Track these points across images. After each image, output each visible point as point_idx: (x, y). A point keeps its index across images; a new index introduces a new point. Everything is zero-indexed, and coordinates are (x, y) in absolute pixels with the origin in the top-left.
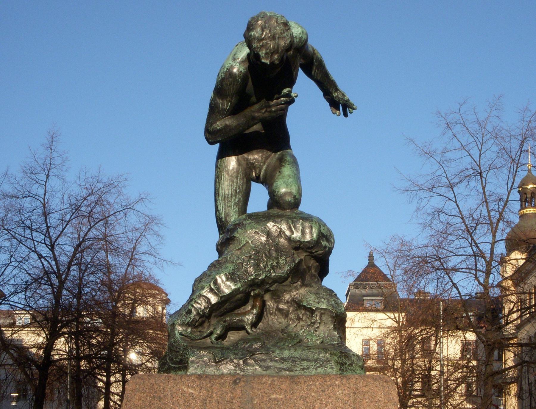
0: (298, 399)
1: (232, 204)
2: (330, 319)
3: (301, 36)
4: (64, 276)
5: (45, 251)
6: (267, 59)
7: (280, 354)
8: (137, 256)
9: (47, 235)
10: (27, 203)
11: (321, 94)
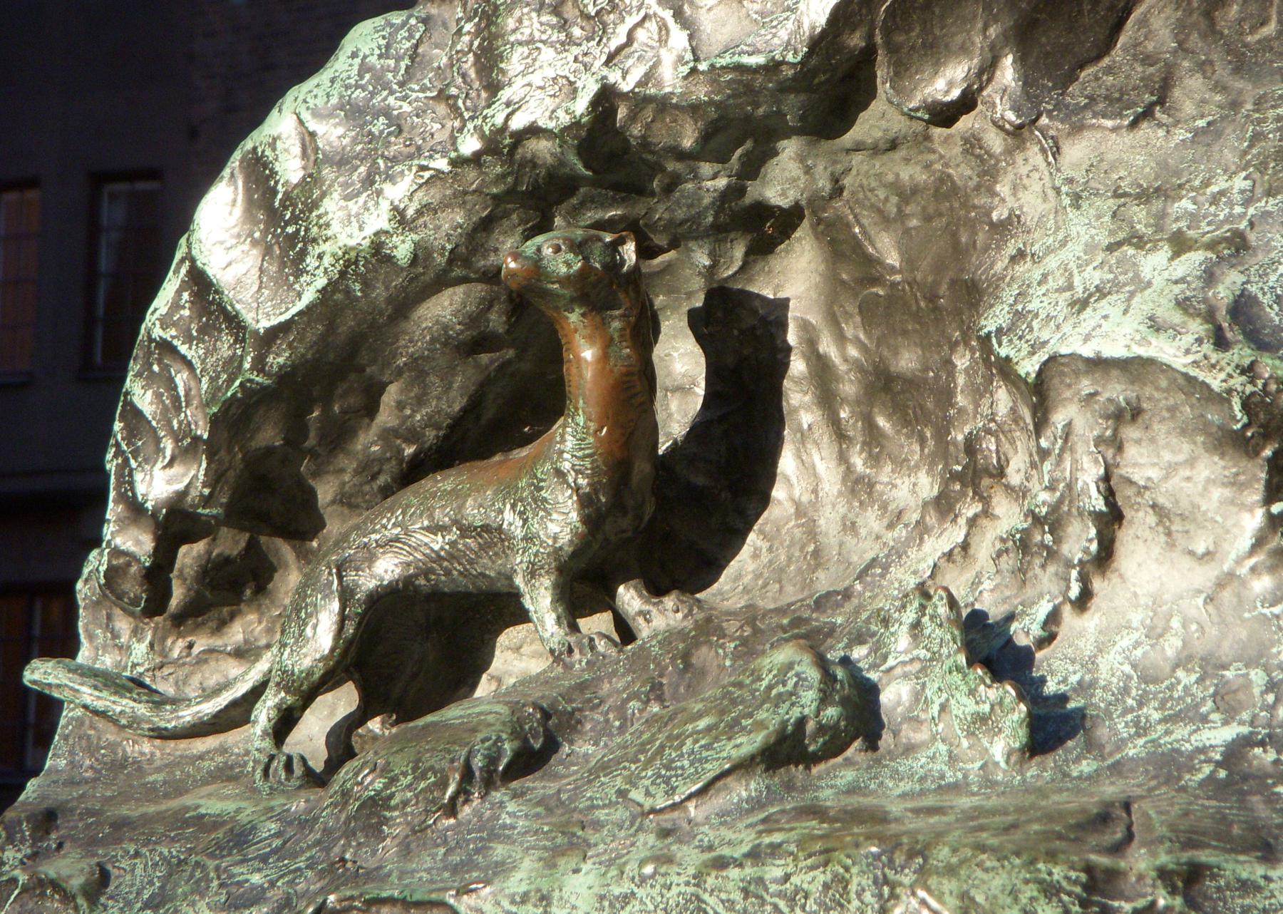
2: (1211, 467)
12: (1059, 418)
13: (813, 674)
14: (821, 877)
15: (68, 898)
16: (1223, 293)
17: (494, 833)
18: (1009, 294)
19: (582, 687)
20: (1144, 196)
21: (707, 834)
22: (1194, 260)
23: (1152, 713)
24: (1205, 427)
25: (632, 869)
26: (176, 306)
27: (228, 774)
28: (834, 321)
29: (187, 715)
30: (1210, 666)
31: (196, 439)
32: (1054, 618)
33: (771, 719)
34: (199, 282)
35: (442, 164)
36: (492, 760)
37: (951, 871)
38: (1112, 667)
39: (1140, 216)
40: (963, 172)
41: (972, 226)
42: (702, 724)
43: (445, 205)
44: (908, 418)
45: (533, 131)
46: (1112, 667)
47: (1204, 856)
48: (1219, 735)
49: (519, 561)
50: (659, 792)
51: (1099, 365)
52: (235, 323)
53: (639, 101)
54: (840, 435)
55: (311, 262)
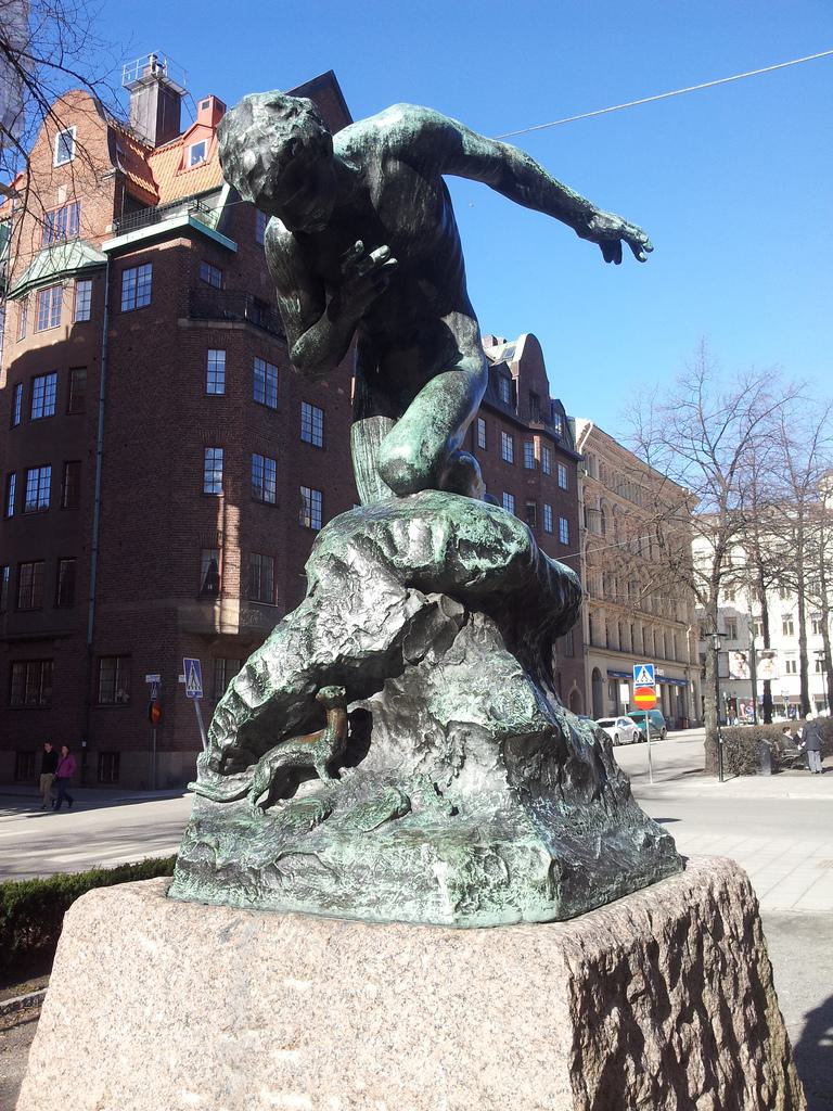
0: (338, 998)
1: (379, 486)
2: (486, 746)
3: (402, 126)
4: (727, 481)
5: (706, 459)
6: (247, 192)
7: (336, 856)
8: (821, 445)
9: (705, 441)
10: (683, 413)
11: (572, 231)
12: (452, 734)
13: (399, 796)
14: (413, 851)
15: (211, 848)
16: (488, 706)
17: (323, 835)
18: (436, 703)
19: (335, 794)
20: (465, 681)
21: (380, 838)
22: (480, 698)
23: (478, 804)
24: (485, 737)
25: (363, 847)
26: (229, 700)
27: (240, 810)
28: (387, 703)
29: (229, 795)
30: (489, 792)
31: (234, 732)
32: (451, 779)
33: (391, 808)
34: (236, 696)
35: (299, 670)
36: (320, 816)
37: (445, 850)
38: (466, 792)
39: (465, 686)
40: (421, 672)
41: (423, 685)
42: (373, 808)
43: (300, 680)
44: (407, 726)
45: (322, 664)
46: (466, 792)
47: (499, 842)
48: (494, 809)
49: (316, 761)
50: (366, 826)
51: (461, 723)
52: (246, 706)
53: (347, 658)
54: (389, 728)
55: (266, 692)
